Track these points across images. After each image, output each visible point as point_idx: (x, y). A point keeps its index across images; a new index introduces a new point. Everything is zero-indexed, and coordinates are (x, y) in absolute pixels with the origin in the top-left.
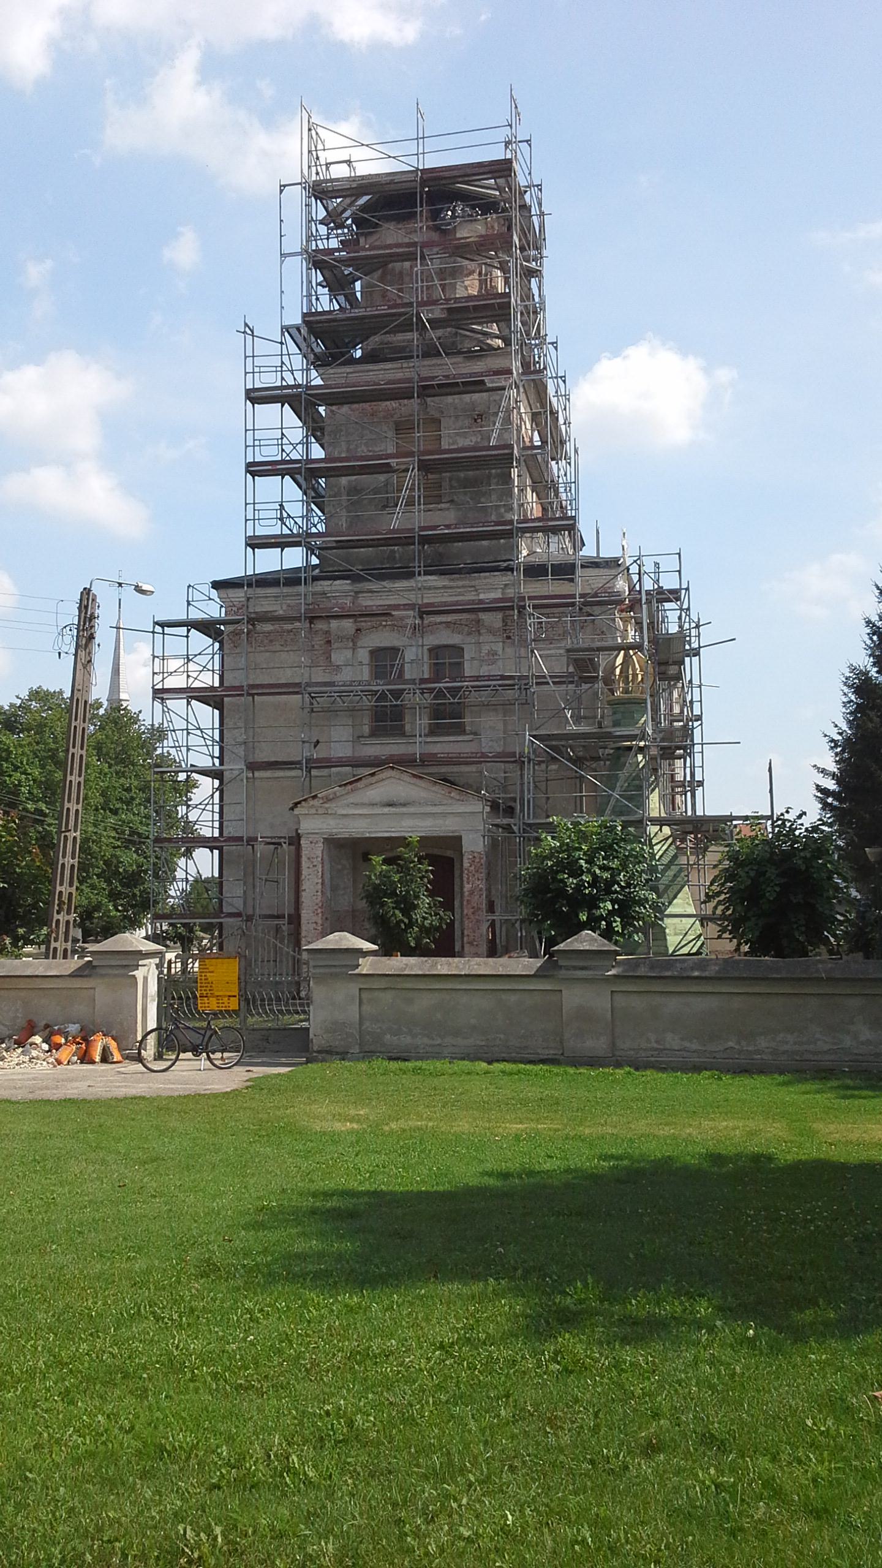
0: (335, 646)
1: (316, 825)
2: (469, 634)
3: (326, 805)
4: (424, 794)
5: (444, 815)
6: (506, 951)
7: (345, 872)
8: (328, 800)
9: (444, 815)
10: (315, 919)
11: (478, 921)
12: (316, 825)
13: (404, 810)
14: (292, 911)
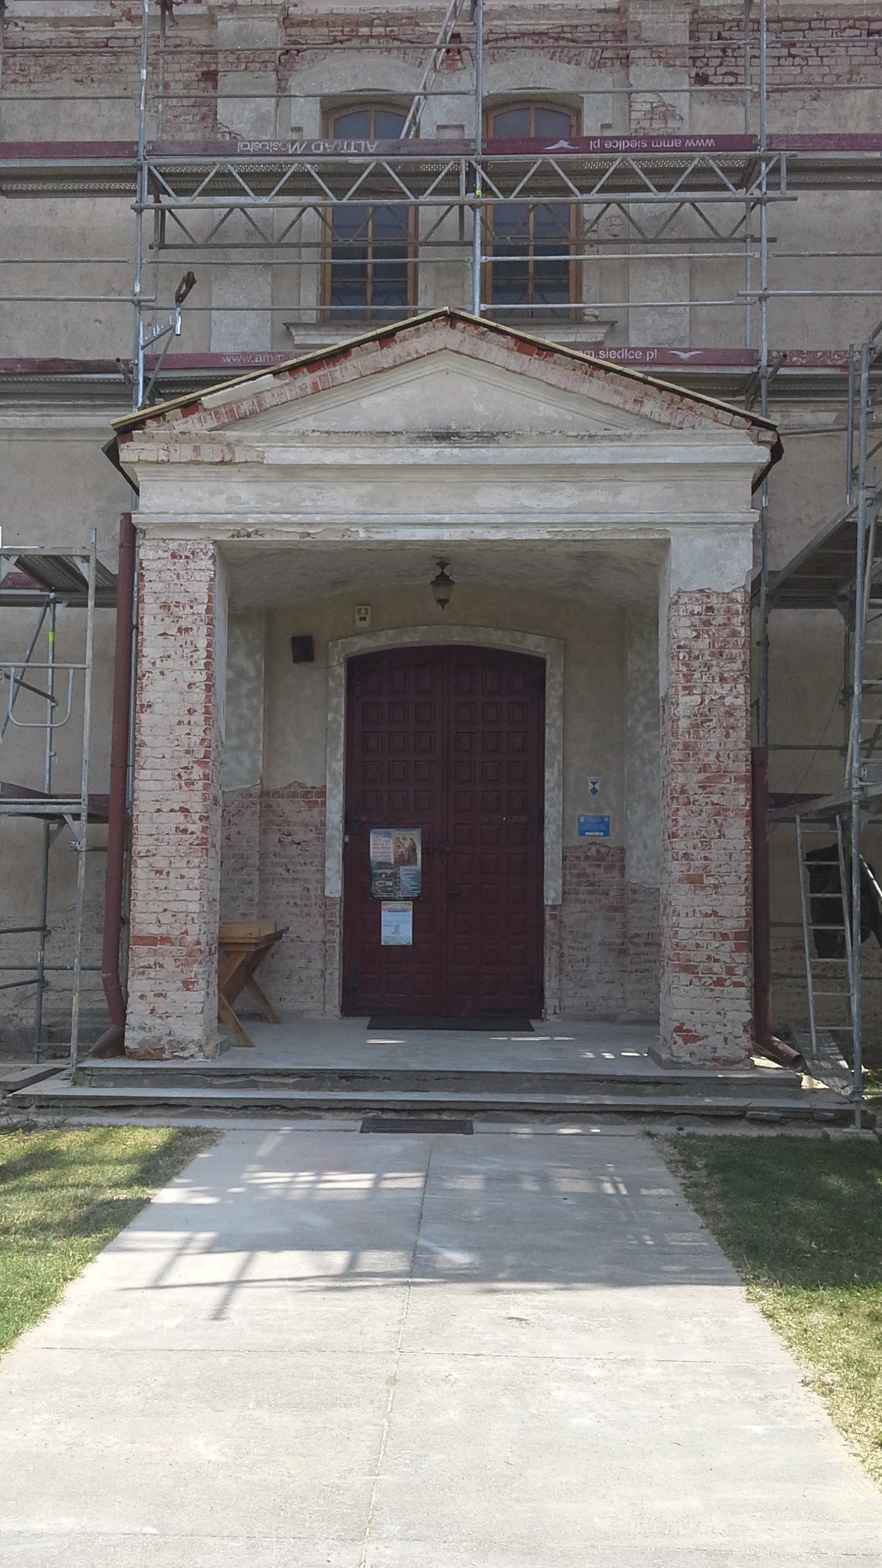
0: (226, 82)
1: (197, 497)
2: (598, 65)
3: (231, 435)
4: (546, 409)
5: (614, 473)
6: (81, 1085)
7: (246, 687)
8: (238, 419)
9: (614, 473)
10: (180, 798)
11: (720, 811)
12: (197, 497)
13: (487, 454)
14: (105, 789)
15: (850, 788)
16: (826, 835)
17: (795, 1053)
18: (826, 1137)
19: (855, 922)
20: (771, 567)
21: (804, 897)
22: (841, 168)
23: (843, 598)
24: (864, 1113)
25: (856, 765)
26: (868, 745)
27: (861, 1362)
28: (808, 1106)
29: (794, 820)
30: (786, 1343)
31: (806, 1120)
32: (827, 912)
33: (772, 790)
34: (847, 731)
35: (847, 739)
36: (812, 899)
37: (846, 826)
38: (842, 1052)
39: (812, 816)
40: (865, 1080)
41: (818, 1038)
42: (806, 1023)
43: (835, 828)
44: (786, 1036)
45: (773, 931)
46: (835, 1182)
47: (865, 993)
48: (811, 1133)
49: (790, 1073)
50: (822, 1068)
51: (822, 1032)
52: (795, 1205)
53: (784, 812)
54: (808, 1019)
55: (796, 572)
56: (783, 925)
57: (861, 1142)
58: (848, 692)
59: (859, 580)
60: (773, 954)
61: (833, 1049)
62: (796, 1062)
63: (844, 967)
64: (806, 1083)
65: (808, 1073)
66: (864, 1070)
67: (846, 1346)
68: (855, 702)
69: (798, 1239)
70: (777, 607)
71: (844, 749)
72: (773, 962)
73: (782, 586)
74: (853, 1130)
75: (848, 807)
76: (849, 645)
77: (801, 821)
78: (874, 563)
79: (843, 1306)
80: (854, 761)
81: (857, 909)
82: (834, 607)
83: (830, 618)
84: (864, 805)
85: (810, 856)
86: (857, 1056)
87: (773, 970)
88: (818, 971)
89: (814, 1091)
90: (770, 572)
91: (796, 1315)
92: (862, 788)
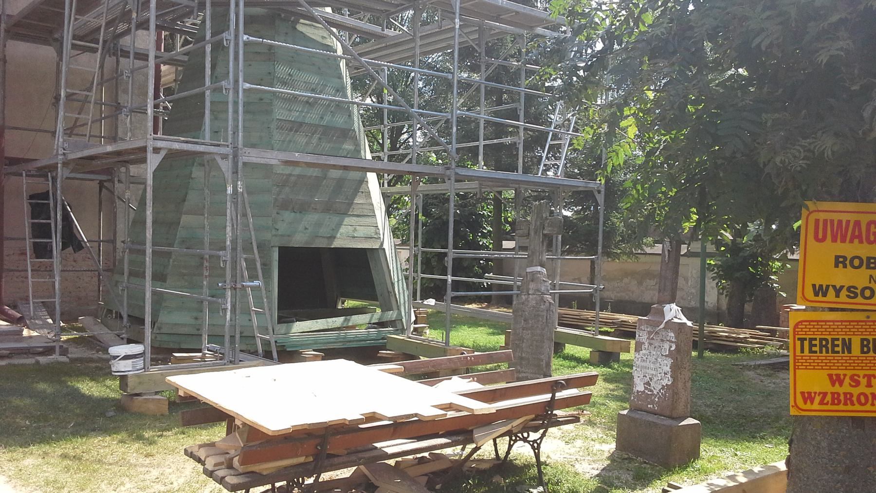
15: (57, 154)
16: (41, 185)
17: (19, 315)
18: (38, 362)
19: (58, 235)
20: (8, 12)
21: (27, 222)
22: (341, 166)
23: (56, 40)
24: (61, 347)
25: (61, 140)
26: (68, 132)
27: (55, 481)
28: (26, 346)
29: (21, 175)
30: (8, 479)
31: (25, 353)
32: (42, 231)
33: (6, 155)
34: (56, 122)
35: (56, 127)
36: (33, 224)
37: (54, 179)
38: (49, 314)
39: (33, 173)
40: (63, 329)
41: (35, 308)
42: (27, 299)
43: (48, 180)
44: (14, 307)
45: (6, 243)
46: (42, 386)
47: (63, 280)
48: (30, 361)
49: (15, 328)
50: (36, 324)
51: (37, 303)
52: (16, 401)
53: (14, 169)
54: (28, 296)
55: (25, 17)
56: (12, 239)
57: (59, 363)
58: (57, 98)
59: (65, 31)
60: (6, 258)
61: (43, 313)
62: (20, 321)
63: (52, 265)
64: (26, 332)
65: (28, 328)
66: (62, 324)
67: (47, 474)
68: (61, 102)
69: (17, 420)
70: (12, 39)
71: (54, 133)
72: (5, 262)
73: (15, 25)
74: (55, 357)
75: (54, 167)
76: (59, 71)
77: (27, 175)
78: (76, 19)
79: (46, 453)
80: (60, 138)
81: (60, 227)
82: (50, 45)
83: (47, 52)
84: (65, 164)
85: (31, 197)
86: (58, 316)
87: (5, 267)
88: (36, 268)
89: (31, 337)
90: (8, 15)
91: (15, 463)
92: (64, 154)
